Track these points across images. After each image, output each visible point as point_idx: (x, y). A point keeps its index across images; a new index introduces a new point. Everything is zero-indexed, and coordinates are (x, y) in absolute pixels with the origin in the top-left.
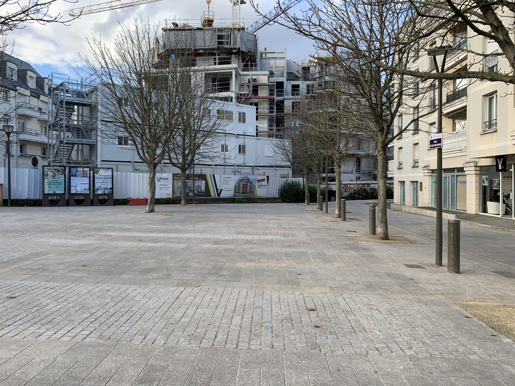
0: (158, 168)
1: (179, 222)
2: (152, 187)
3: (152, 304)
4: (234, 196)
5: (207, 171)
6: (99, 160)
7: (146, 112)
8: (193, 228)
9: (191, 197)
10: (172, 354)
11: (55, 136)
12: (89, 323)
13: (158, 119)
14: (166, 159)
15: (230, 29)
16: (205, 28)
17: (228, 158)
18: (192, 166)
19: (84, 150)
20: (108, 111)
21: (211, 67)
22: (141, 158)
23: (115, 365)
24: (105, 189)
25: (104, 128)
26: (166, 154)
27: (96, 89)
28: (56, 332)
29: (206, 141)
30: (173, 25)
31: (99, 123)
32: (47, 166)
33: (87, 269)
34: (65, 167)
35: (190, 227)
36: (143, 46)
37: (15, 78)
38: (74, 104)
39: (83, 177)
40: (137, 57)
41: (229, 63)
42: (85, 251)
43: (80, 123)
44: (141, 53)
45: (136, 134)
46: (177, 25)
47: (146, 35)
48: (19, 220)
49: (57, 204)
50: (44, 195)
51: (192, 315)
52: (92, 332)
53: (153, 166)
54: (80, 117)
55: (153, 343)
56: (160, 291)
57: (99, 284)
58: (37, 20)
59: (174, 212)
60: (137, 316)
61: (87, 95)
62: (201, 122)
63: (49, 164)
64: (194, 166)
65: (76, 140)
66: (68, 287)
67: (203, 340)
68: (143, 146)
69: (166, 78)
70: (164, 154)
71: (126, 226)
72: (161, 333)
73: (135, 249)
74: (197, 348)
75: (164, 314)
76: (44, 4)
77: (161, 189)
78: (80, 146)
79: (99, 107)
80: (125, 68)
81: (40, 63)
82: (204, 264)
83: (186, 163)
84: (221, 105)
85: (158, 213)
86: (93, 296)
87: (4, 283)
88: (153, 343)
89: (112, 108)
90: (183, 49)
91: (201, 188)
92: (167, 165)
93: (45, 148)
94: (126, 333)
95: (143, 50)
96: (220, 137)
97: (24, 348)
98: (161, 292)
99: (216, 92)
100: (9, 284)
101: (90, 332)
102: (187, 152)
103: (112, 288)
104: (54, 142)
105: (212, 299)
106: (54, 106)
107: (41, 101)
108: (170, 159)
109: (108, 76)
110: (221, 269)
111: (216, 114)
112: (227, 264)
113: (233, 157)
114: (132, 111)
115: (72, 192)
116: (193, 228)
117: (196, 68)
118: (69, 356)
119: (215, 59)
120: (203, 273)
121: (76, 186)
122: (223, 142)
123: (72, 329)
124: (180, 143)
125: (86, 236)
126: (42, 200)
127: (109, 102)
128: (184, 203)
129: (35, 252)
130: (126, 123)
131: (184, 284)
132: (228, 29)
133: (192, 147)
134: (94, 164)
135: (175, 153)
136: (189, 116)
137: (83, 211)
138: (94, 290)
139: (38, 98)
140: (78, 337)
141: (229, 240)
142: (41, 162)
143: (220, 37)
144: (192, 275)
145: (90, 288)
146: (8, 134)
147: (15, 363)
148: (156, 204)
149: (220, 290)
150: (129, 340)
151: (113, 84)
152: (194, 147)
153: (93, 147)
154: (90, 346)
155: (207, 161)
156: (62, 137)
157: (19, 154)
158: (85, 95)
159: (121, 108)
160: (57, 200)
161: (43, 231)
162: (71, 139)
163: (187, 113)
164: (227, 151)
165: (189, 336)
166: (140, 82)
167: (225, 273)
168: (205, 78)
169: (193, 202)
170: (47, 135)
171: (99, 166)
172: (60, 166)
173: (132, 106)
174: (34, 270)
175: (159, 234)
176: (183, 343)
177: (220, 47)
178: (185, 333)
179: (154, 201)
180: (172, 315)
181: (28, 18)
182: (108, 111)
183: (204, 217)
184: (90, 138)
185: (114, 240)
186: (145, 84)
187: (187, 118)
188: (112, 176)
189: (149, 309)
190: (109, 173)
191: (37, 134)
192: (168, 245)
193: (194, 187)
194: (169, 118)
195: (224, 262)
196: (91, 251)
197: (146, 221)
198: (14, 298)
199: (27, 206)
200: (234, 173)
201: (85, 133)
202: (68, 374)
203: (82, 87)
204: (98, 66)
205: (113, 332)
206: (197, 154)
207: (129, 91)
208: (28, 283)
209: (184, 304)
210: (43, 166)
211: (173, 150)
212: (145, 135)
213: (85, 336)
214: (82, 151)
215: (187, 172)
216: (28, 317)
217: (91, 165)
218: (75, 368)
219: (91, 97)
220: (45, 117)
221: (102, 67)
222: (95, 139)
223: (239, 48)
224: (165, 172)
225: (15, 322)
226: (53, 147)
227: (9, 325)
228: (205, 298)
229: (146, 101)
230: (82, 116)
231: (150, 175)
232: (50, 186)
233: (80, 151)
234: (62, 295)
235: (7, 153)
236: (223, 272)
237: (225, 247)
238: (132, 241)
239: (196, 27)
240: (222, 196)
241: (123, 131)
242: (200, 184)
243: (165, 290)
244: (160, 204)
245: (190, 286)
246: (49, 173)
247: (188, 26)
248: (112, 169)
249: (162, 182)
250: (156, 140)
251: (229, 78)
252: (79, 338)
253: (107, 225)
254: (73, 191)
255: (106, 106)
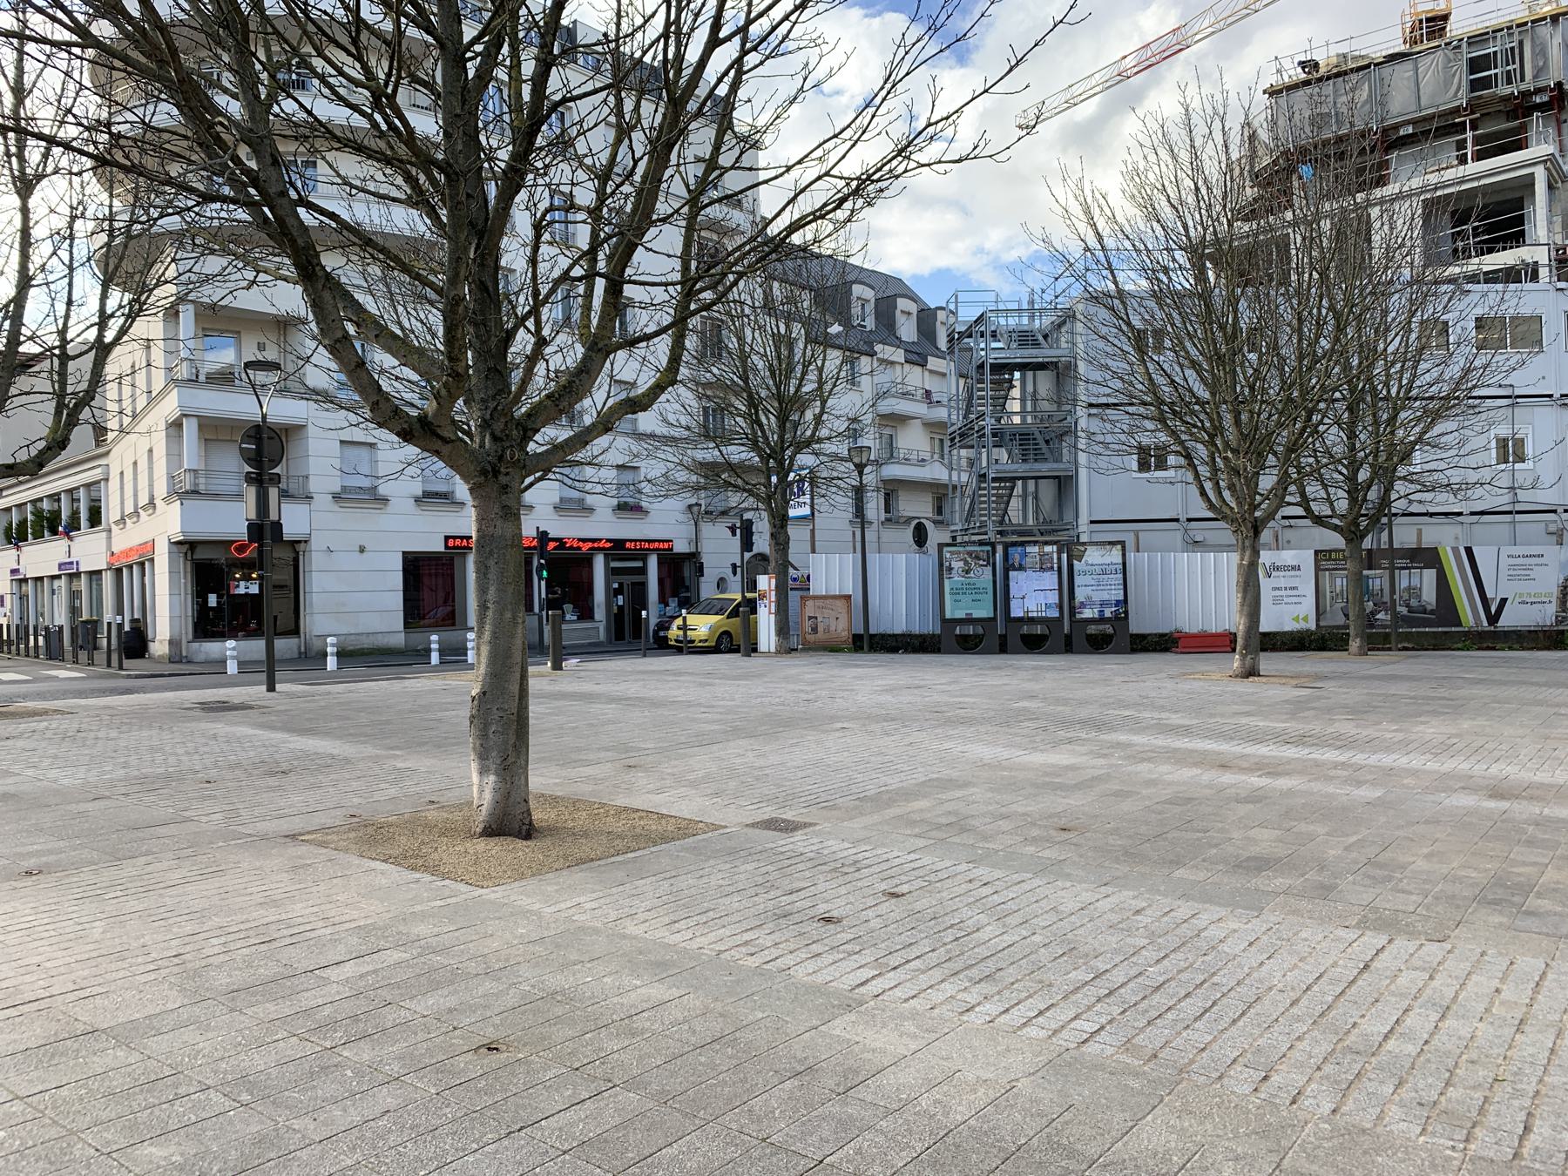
0: (1266, 536)
1: (1348, 713)
2: (1249, 596)
3: (1278, 975)
4: (1558, 622)
5: (1442, 537)
6: (1084, 519)
7: (1222, 361)
8: (1400, 736)
9: (1385, 627)
10: (1365, 1153)
11: (964, 462)
12: (1094, 1000)
13: (1264, 380)
14: (1289, 504)
15: (1518, 26)
16: (1417, 49)
17: (1528, 483)
18: (1385, 520)
19: (1040, 495)
20: (1108, 377)
21: (1450, 174)
22: (1211, 506)
23: (1180, 1146)
24: (1103, 604)
25: (1095, 425)
26: (1292, 488)
27: (1069, 316)
28: (1008, 1010)
29: (1437, 430)
30: (1303, 68)
31: (1081, 412)
32: (948, 545)
33: (1075, 840)
34: (993, 545)
35: (1388, 731)
36: (1208, 160)
37: (870, 323)
38: (1011, 368)
39: (1042, 569)
40: (1191, 200)
41: (1519, 145)
42: (1061, 787)
43: (1029, 420)
44: (1200, 183)
45: (1192, 434)
46: (1316, 65)
47: (1217, 125)
48: (889, 690)
49: (977, 646)
50: (944, 621)
51: (1426, 1036)
52: (1102, 1028)
53: (1250, 530)
54: (1029, 403)
55: (1294, 1102)
56: (1303, 935)
57: (1109, 889)
58: (929, 165)
59: (1325, 678)
60: (1233, 1005)
61: (1045, 337)
62: (1415, 368)
63: (954, 538)
64: (1390, 521)
65: (1021, 468)
66: (1026, 886)
67: (1477, 1130)
68: (1215, 470)
69: (1283, 245)
70: (1286, 488)
71: (1176, 719)
72: (1319, 1074)
73: (1208, 792)
74: (1455, 1155)
75: (1322, 1015)
76: (947, 118)
77: (1277, 601)
78: (1031, 483)
79: (1082, 367)
80: (1153, 236)
81: (925, 270)
82: (1455, 864)
83: (1363, 512)
84: (1493, 299)
85: (1272, 679)
86: (1098, 922)
87: (875, 852)
88: (1294, 1102)
89: (1120, 366)
90: (1340, 140)
91: (1420, 596)
92: (1293, 522)
93: (940, 494)
94: (1203, 1050)
95: (1207, 173)
96: (1491, 413)
97: (934, 1036)
98: (1306, 940)
99: (1470, 257)
100: (885, 857)
101: (1098, 1026)
102: (1363, 475)
103: (1150, 906)
104: (964, 477)
105: (1497, 991)
106: (962, 382)
107: (931, 372)
108: (1305, 502)
109: (1105, 273)
110: (1526, 889)
111: (1474, 333)
112: (1551, 875)
113: (1547, 478)
114: (1181, 366)
115: (1013, 615)
116: (1400, 736)
117: (1390, 189)
118: (1046, 1085)
119: (1461, 145)
120: (1454, 896)
121: (1023, 598)
122: (1503, 430)
123: (1048, 1009)
124: (1339, 450)
125: (1061, 742)
126: (939, 636)
127: (1109, 349)
128: (1360, 647)
129: (935, 776)
130: (1163, 402)
131: (1390, 925)
132: (1509, 28)
133: (1383, 457)
134: (1071, 533)
135: (1323, 483)
136: (1370, 354)
137: (1048, 669)
138: (1097, 904)
139: (923, 365)
140: (1064, 1034)
141: (1552, 786)
142: (935, 536)
143: (1475, 65)
144: (1414, 898)
145: (1087, 897)
146: (860, 468)
147: (918, 1071)
148: (1263, 650)
149: (1530, 964)
150: (1215, 1075)
151: (1121, 294)
152: (1389, 458)
153: (1065, 485)
154: (1102, 1067)
155: (1443, 501)
156: (984, 464)
157: (883, 516)
158: (1041, 338)
159: (1144, 362)
160: (976, 636)
161: (950, 722)
162: (1007, 468)
163: (1361, 346)
164: (1521, 458)
165: (1421, 1104)
166: (1201, 277)
167: (1545, 904)
168: (1426, 221)
169: (1393, 645)
170: (946, 461)
171: (1084, 538)
172: (981, 543)
173: (1178, 348)
174: (939, 827)
175: (1284, 748)
176: (1400, 1124)
177: (1480, 97)
178: (1406, 1093)
179: (1256, 642)
180: (1351, 1021)
181: (912, 165)
182: (1108, 377)
183: (1444, 698)
184: (1058, 460)
185: (1143, 760)
186: (1218, 276)
187: (1360, 363)
188: (1124, 564)
189: (1270, 989)
190: (1115, 556)
191: (923, 460)
192: (1316, 786)
193: (1393, 591)
194: (1301, 368)
195: (1535, 864)
196: (1078, 786)
197: (1236, 704)
198: (898, 896)
199: (906, 651)
200: (1554, 538)
201: (1043, 445)
202: (1049, 1136)
203: (1032, 318)
204: (1076, 250)
205: (1164, 1040)
206: (1404, 478)
207: (1169, 306)
208: (926, 860)
209: (1393, 994)
210: (941, 546)
211: (1316, 474)
212: (1222, 435)
213: (1085, 1036)
214: (1036, 498)
215: (1367, 543)
216: (935, 954)
217: (1062, 536)
218: (1067, 1123)
219: (1058, 340)
220: (941, 413)
221: (1087, 249)
222: (1072, 460)
223: (1559, 85)
224: (1289, 545)
225: (908, 961)
226: (963, 495)
227: (895, 968)
228: (1470, 984)
229: (1222, 327)
230: (1035, 400)
231: (1242, 559)
232: (958, 597)
233: (1030, 499)
234: (1011, 905)
235: (857, 517)
236: (1533, 902)
237: (1535, 809)
238: (1196, 765)
239: (1384, 54)
240: (1505, 621)
241: (1153, 428)
242: (1415, 582)
243: (1320, 937)
244: (1274, 649)
245: (1411, 934)
246: (954, 564)
247: (1355, 58)
248: (1123, 543)
249: (1280, 579)
250: (1255, 446)
251: (1521, 199)
252: (1068, 1038)
253: (1117, 712)
254: (1016, 612)
255: (1102, 362)
